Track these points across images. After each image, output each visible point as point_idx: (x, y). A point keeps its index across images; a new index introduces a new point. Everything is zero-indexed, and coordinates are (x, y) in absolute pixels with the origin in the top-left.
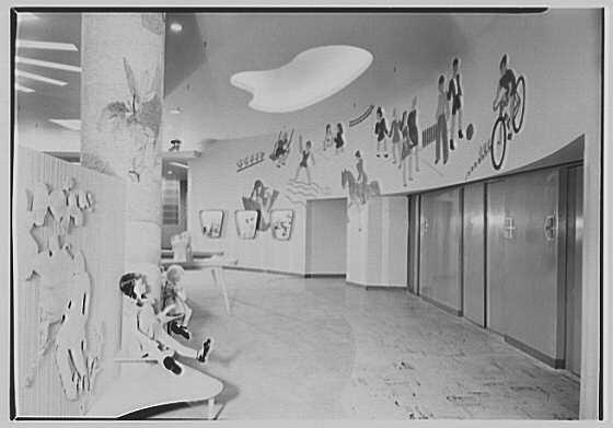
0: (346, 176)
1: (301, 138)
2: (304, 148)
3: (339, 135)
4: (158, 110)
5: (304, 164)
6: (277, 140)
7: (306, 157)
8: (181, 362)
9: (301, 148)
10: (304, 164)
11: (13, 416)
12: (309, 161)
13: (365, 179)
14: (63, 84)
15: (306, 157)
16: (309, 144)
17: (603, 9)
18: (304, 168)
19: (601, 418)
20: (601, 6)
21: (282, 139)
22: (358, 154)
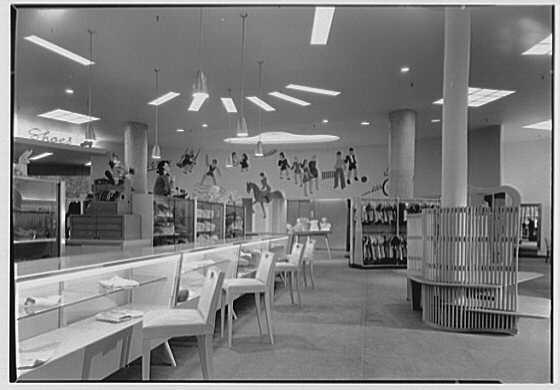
0: (250, 186)
1: (207, 157)
2: (211, 163)
3: (245, 160)
4: (166, 188)
5: (210, 173)
6: (183, 153)
7: (212, 169)
8: (94, 122)
9: (207, 164)
10: (210, 173)
11: (13, 378)
12: (214, 172)
13: (269, 189)
14: (86, 62)
15: (212, 169)
16: (215, 161)
17: (553, 7)
18: (210, 177)
19: (552, 382)
20: (551, 4)
21: (189, 153)
22: (262, 175)
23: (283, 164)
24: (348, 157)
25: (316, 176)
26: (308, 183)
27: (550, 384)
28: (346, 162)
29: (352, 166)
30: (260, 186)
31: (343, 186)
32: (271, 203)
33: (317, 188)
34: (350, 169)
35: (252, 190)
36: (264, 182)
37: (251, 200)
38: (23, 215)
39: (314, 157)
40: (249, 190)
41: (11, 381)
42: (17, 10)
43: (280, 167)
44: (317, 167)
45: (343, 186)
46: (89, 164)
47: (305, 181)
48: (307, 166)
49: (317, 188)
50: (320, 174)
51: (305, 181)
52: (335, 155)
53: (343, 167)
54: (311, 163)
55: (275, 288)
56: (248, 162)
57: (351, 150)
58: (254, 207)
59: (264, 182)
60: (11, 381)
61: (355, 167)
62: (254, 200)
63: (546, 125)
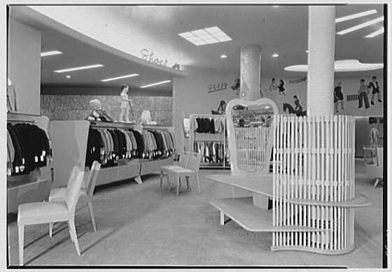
24: (371, 84)
28: (369, 87)
34: (374, 93)
35: (287, 109)
36: (297, 103)
42: (10, 7)
49: (343, 108)
53: (366, 91)
57: (374, 78)
59: (297, 103)
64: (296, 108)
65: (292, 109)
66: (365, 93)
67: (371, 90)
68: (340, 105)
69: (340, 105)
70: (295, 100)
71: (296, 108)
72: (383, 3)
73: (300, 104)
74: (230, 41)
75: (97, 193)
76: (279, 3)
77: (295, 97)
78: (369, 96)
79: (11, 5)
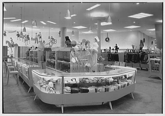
19: (162, 113)
23: (18, 35)
24: (39, 35)
25: (29, 40)
26: (27, 42)
27: (162, 114)
28: (38, 36)
29: (40, 37)
30: (11, 42)
31: (38, 43)
32: (14, 47)
33: (30, 43)
34: (40, 38)
35: (8, 43)
36: (12, 40)
37: (7, 46)
38: (33, 35)
39: (29, 34)
40: (6, 43)
41: (3, 113)
42: (4, 4)
43: (17, 36)
44: (29, 37)
45: (38, 43)
46: (97, 24)
47: (25, 41)
48: (26, 36)
49: (30, 43)
50: (30, 39)
51: (25, 41)
52: (35, 34)
53: (38, 37)
54: (27, 36)
55: (93, 53)
56: (6, 34)
57: (40, 33)
58: (8, 49)
59: (12, 40)
60: (3, 113)
61: (41, 38)
62: (8, 47)
63: (161, 21)
64: (11, 43)
65: (10, 43)
66: (37, 38)
67: (39, 37)
68: (29, 42)
69: (29, 42)
70: (11, 39)
71: (11, 43)
72: (162, 2)
73: (13, 41)
74: (70, 19)
75: (107, 103)
76: (54, 2)
77: (11, 38)
78: (39, 39)
79: (5, 3)
